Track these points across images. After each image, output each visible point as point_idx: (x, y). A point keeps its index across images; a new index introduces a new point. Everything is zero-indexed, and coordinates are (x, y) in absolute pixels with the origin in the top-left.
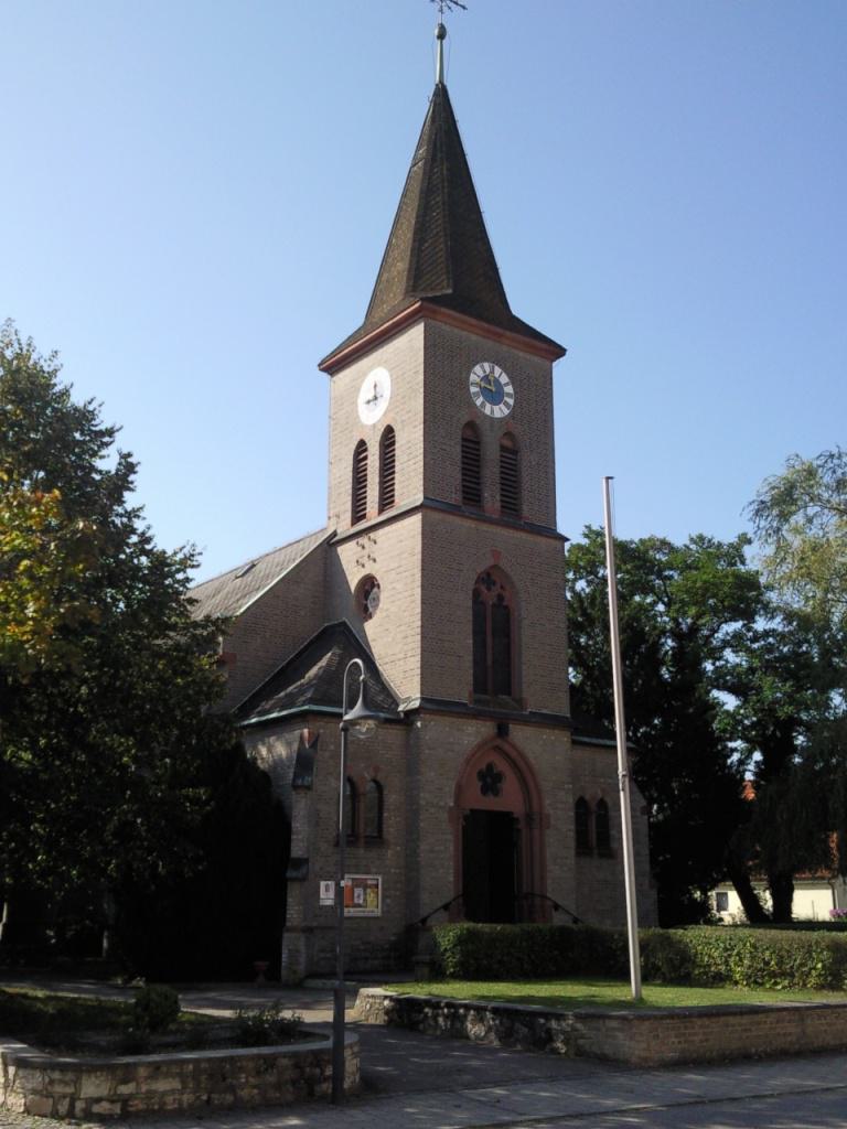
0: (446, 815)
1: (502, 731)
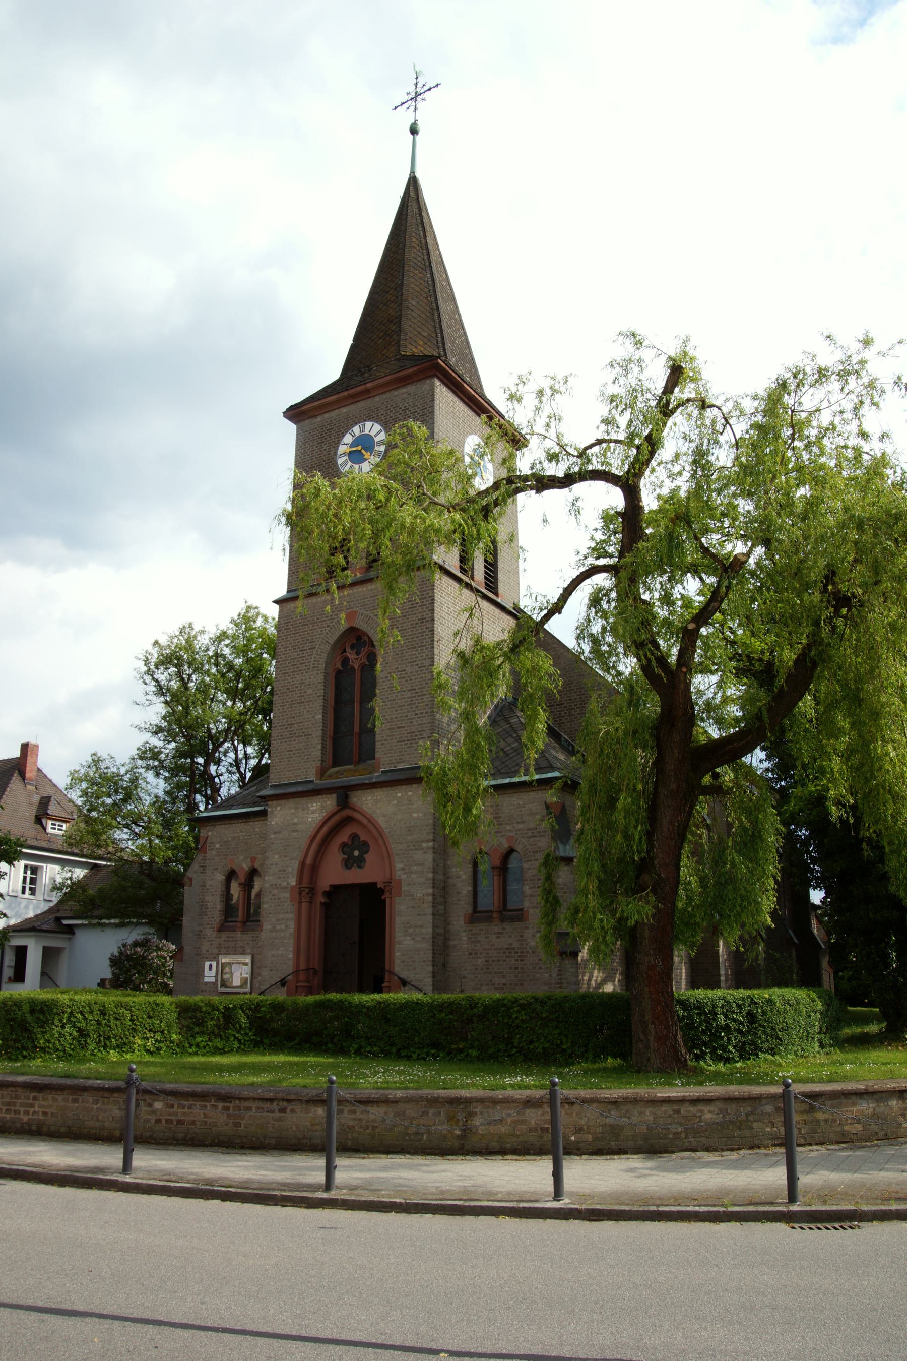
0: (288, 895)
1: (344, 802)
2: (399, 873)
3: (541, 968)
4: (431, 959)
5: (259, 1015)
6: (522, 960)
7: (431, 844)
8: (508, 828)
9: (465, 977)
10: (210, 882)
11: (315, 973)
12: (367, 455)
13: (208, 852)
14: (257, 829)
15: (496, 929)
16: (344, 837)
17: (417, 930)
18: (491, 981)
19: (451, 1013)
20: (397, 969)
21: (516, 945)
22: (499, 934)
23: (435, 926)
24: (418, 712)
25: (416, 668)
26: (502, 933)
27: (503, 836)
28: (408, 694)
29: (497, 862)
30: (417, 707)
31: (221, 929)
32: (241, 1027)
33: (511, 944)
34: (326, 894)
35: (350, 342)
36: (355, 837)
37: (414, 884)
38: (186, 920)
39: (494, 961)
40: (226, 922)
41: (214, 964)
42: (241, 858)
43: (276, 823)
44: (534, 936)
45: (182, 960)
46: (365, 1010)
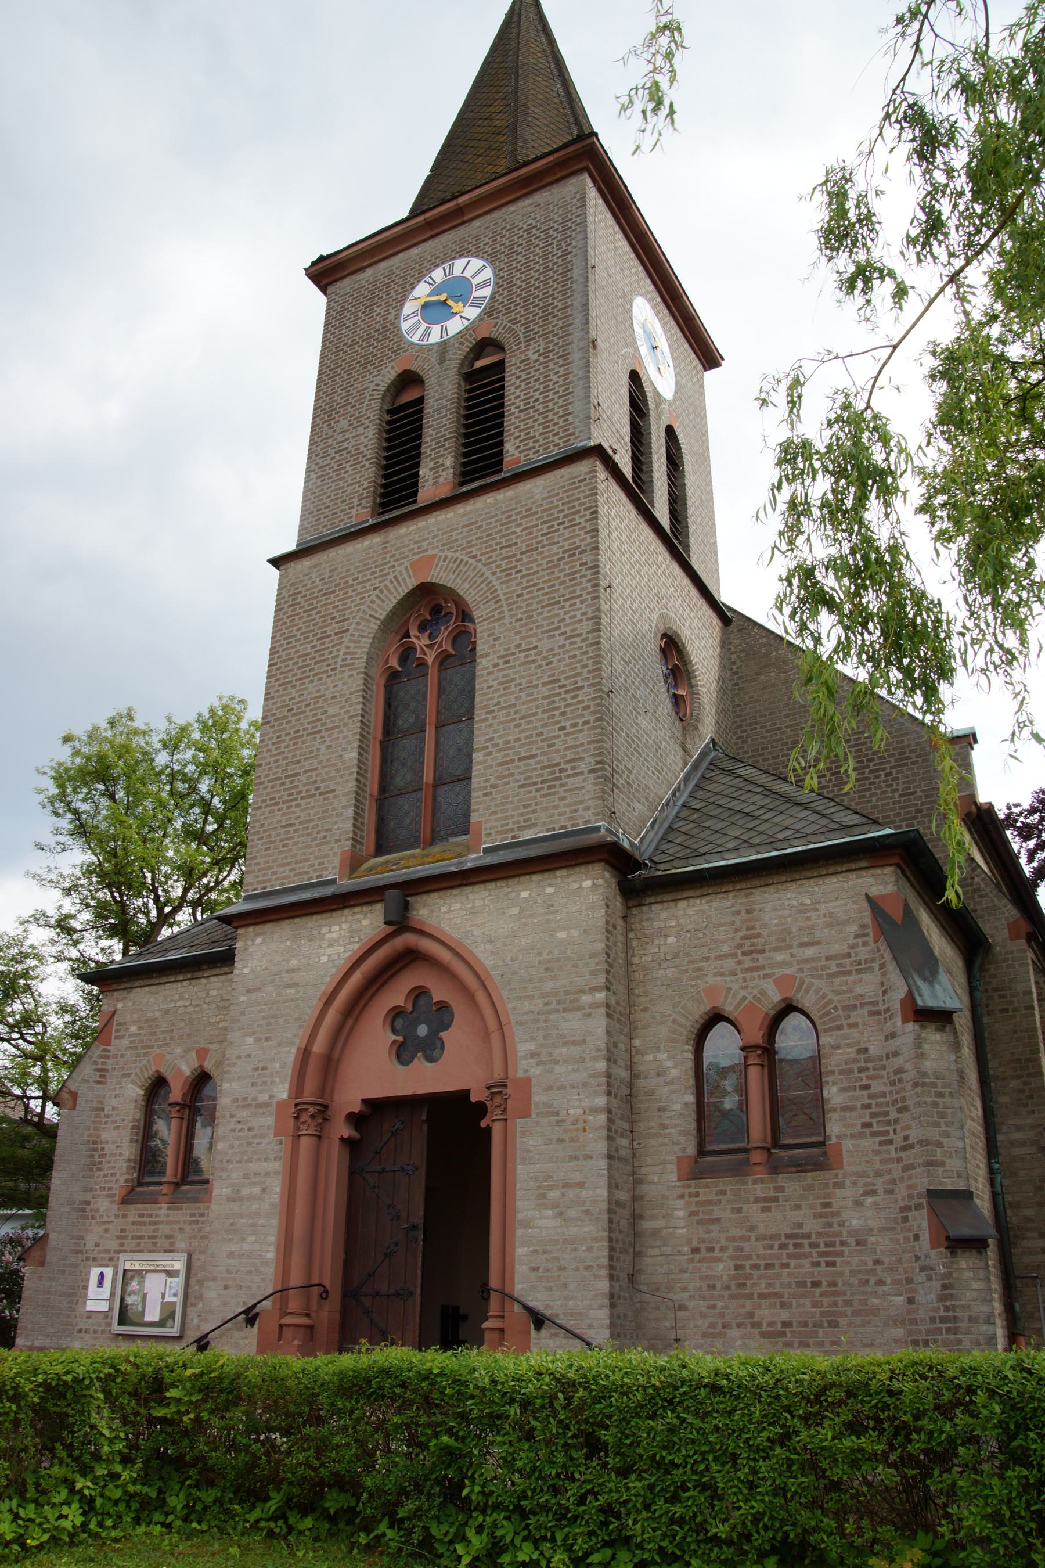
0: (270, 1121)
2: (523, 1064)
3: (881, 1282)
4: (605, 1261)
5: (159, 1412)
6: (833, 1264)
7: (601, 996)
8: (779, 957)
9: (682, 1307)
10: (114, 1102)
11: (325, 1295)
12: (456, 307)
13: (114, 1042)
14: (214, 993)
15: (760, 1190)
16: (396, 995)
17: (571, 1193)
18: (751, 1315)
19: (855, 1427)
20: (520, 1288)
21: (812, 1226)
22: (767, 1203)
23: (613, 1185)
24: (567, 724)
25: (561, 640)
26: (776, 1199)
27: (766, 976)
28: (545, 691)
29: (757, 1037)
30: (563, 714)
31: (128, 1198)
32: (96, 1456)
33: (801, 1226)
34: (355, 1119)
35: (426, 172)
36: (419, 993)
37: (561, 1088)
38: (58, 1179)
39: (755, 1267)
40: (140, 1183)
41: (108, 1272)
42: (179, 1050)
43: (252, 971)
44: (858, 1203)
45: (42, 1264)
46: (514, 1410)
